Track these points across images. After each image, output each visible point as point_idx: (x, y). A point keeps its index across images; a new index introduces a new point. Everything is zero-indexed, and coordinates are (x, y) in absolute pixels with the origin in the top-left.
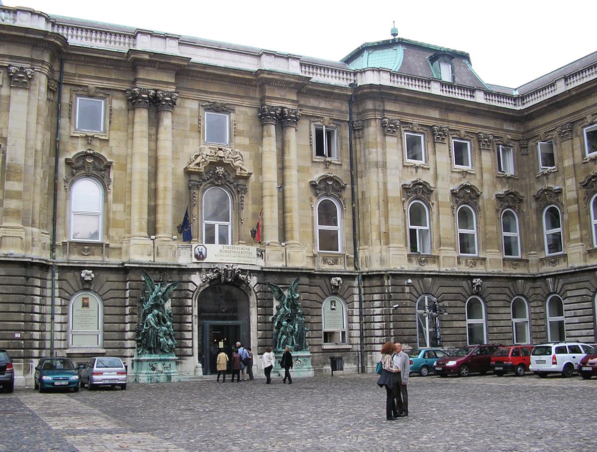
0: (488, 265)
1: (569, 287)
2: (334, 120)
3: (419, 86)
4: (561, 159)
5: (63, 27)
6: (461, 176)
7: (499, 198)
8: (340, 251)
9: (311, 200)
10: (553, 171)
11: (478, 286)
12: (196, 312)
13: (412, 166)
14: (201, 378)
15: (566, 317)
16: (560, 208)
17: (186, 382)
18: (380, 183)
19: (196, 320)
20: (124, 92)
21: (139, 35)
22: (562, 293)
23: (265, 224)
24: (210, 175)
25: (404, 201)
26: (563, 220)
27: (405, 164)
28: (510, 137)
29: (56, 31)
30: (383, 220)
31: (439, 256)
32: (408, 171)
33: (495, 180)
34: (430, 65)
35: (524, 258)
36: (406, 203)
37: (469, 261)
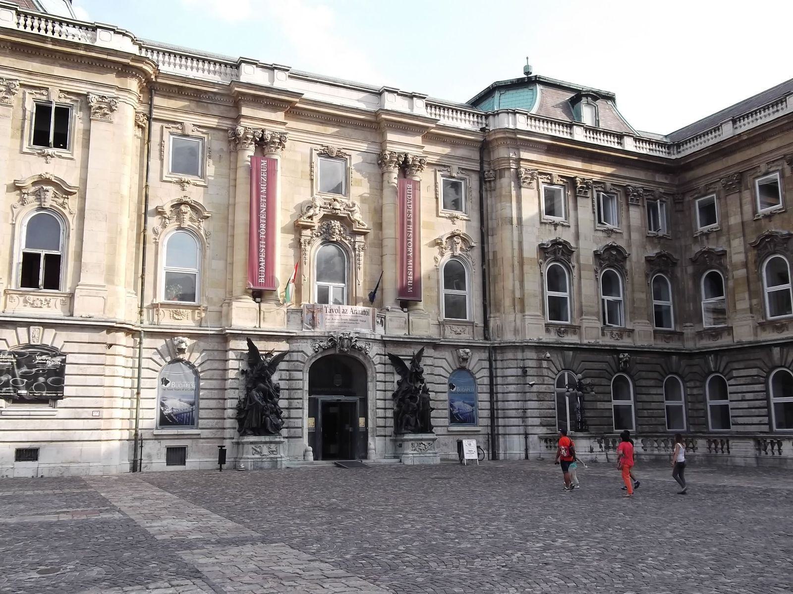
0: (637, 337)
1: (736, 366)
2: (463, 169)
3: (559, 131)
4: (726, 216)
5: (153, 50)
6: (606, 235)
7: (648, 260)
8: (468, 319)
9: (596, 272)
10: (714, 230)
11: (626, 362)
12: (306, 388)
13: (550, 223)
14: (312, 463)
15: (731, 401)
16: (723, 274)
17: (296, 469)
18: (514, 242)
19: (306, 396)
20: (226, 131)
21: (243, 64)
22: (727, 371)
23: (384, 288)
24: (324, 230)
25: (541, 264)
26: (726, 287)
27: (543, 221)
28: (662, 190)
29: (143, 54)
30: (517, 284)
31: (580, 327)
32: (545, 229)
33: (645, 240)
34: (571, 107)
35: (678, 330)
36: (544, 265)
37: (615, 332)
